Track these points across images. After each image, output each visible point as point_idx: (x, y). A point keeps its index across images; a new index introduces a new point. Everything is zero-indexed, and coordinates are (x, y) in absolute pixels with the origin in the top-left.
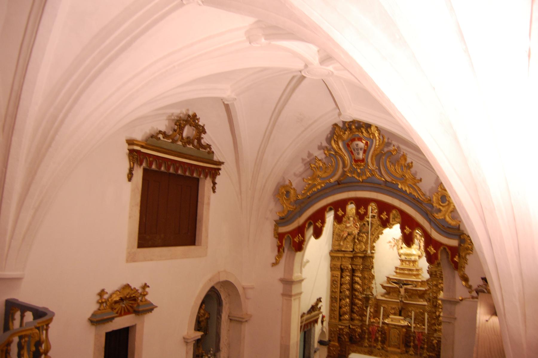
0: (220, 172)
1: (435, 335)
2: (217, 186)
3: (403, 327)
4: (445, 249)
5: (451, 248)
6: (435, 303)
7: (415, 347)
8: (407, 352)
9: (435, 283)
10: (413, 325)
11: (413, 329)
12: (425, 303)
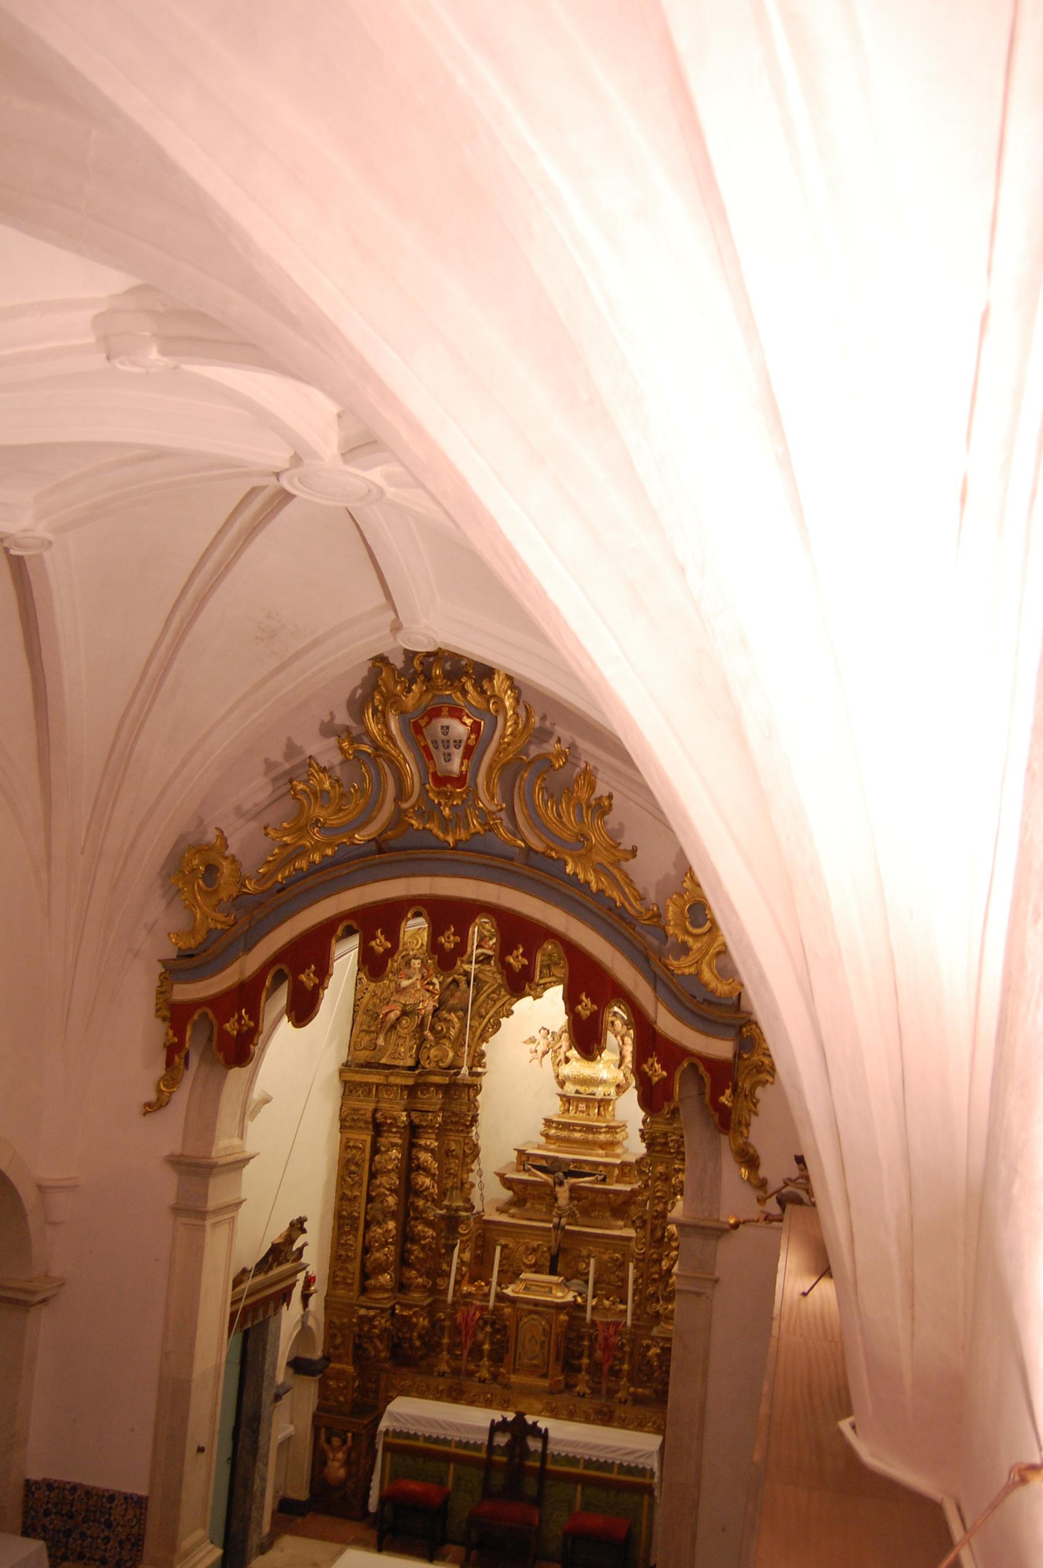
1: (655, 1332)
3: (560, 1307)
4: (693, 1066)
5: (713, 1065)
6: (659, 1233)
7: (595, 1369)
8: (569, 1387)
9: (661, 1169)
10: (592, 1302)
11: (589, 1316)
12: (630, 1232)
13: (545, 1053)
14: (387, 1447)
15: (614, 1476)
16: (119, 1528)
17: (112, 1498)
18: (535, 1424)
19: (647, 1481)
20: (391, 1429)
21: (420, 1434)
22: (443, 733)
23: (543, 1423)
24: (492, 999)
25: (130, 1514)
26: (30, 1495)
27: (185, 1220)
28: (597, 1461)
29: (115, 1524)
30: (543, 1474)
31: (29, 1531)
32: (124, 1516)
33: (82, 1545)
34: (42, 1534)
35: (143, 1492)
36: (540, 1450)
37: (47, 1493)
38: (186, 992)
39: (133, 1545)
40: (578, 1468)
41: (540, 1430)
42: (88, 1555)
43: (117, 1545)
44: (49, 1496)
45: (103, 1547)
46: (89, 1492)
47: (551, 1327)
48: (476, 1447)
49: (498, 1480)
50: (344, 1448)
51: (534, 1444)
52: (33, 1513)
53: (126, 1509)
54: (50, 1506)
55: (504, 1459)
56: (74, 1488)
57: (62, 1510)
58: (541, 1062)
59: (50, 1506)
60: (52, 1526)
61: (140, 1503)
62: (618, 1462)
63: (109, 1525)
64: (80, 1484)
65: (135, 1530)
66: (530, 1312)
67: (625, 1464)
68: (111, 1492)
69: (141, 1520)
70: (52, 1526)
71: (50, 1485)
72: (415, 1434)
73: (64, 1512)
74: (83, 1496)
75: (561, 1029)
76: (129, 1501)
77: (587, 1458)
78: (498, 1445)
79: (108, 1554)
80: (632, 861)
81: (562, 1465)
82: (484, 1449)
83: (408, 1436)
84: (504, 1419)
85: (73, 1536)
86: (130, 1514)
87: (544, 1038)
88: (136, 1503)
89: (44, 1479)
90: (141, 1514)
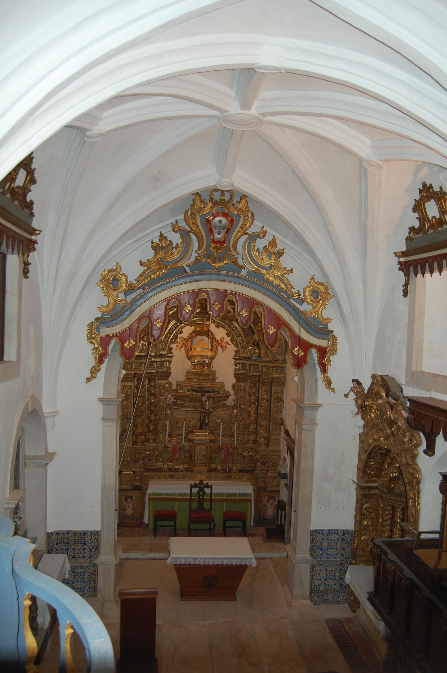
0: (36, 246)
2: (30, 267)
13: (182, 347)
14: (150, 499)
15: (237, 498)
16: (89, 544)
17: (85, 533)
18: (207, 483)
19: (249, 498)
20: (151, 493)
21: (163, 493)
22: (219, 223)
23: (210, 483)
24: (174, 327)
25: (93, 538)
26: (49, 538)
27: (108, 424)
28: (231, 493)
29: (87, 543)
30: (211, 500)
31: (50, 552)
32: (91, 539)
33: (74, 553)
34: (56, 552)
35: (98, 529)
36: (210, 493)
37: (57, 536)
38: (106, 331)
39: (96, 549)
40: (224, 497)
41: (209, 485)
42: (77, 556)
43: (89, 550)
44: (57, 537)
45: (83, 552)
46: (75, 533)
47: (207, 448)
48: (185, 495)
49: (195, 505)
50: (132, 502)
51: (207, 490)
52: (51, 545)
53: (91, 537)
54: (58, 541)
55: (197, 498)
56: (68, 532)
57: (64, 541)
58: (180, 351)
59: (58, 541)
60: (60, 548)
61: (97, 533)
62: (238, 493)
63: (85, 544)
64: (70, 531)
65: (96, 544)
66: (200, 444)
67: (241, 493)
68: (84, 532)
69: (98, 540)
70: (60, 548)
71: (57, 533)
72: (161, 493)
73: (65, 542)
74: (72, 535)
75: (188, 337)
76: (92, 533)
77: (227, 493)
78: (194, 493)
79: (85, 555)
80: (291, 274)
81: (218, 497)
82: (188, 495)
83: (158, 494)
84: (196, 483)
85: (70, 550)
86: (93, 538)
87: (182, 341)
88: (96, 534)
89: (55, 531)
90: (98, 537)
